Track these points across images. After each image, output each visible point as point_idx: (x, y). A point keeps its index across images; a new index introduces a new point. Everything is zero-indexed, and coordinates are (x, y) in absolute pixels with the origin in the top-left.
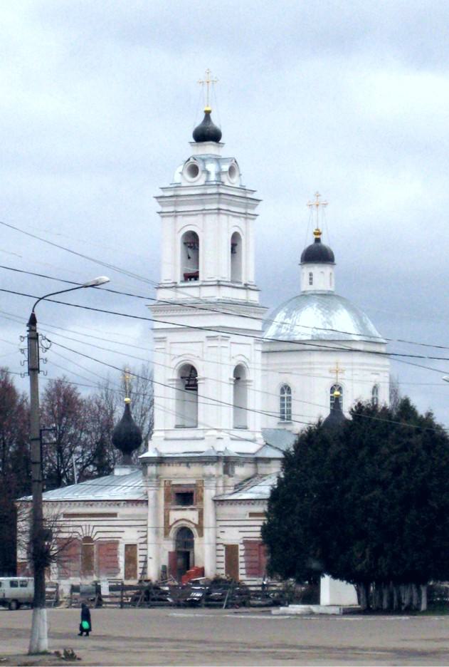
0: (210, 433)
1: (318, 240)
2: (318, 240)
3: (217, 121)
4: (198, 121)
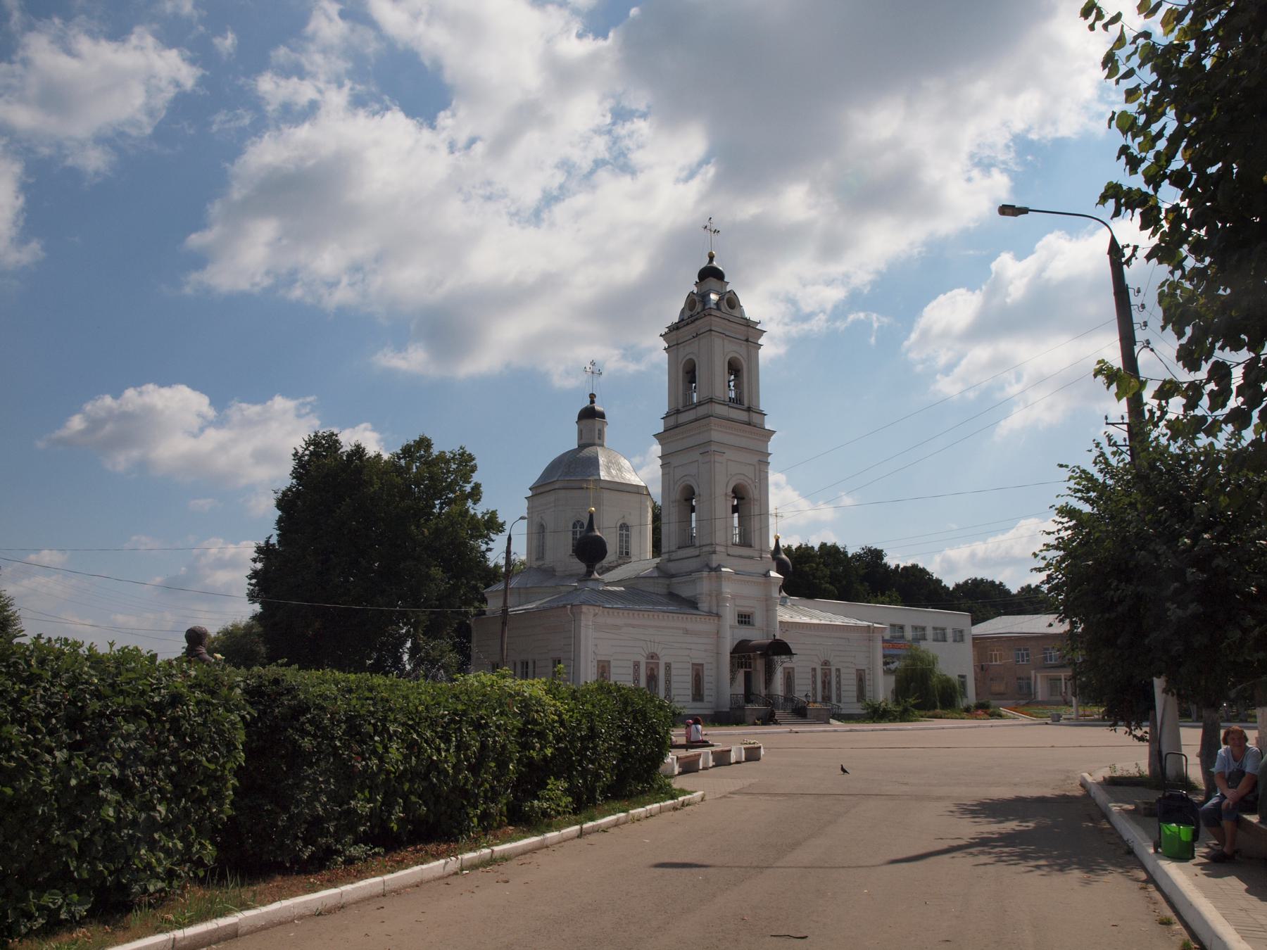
4: (704, 263)
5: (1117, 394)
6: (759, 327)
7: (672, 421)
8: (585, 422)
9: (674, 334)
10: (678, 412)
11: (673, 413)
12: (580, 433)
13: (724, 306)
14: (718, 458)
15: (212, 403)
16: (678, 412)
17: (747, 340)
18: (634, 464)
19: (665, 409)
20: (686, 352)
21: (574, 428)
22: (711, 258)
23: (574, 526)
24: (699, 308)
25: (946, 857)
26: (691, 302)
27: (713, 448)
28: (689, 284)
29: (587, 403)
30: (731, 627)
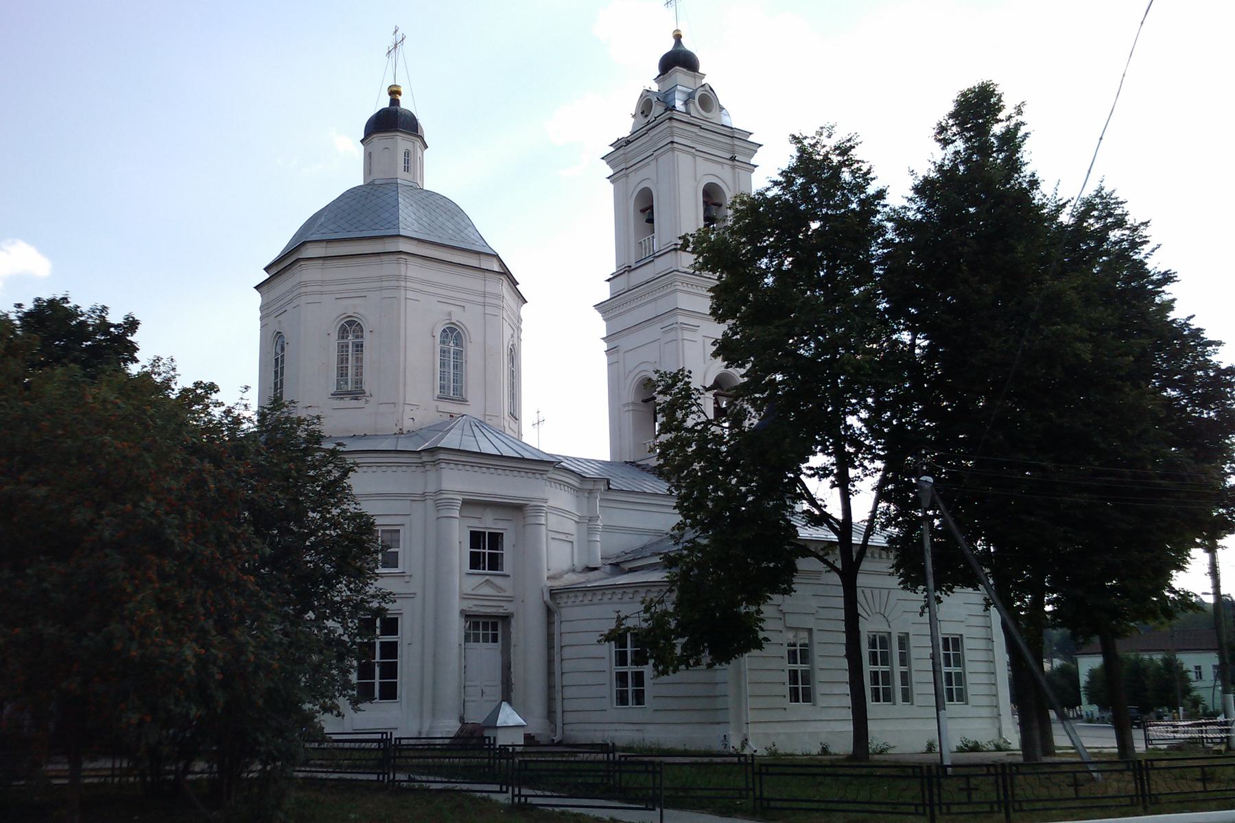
1: (395, 102)
2: (395, 102)
3: (688, 44)
4: (669, 46)
5: (1172, 308)
6: (751, 139)
7: (622, 282)
8: (379, 140)
9: (623, 156)
10: (629, 269)
11: (625, 270)
12: (369, 157)
13: (696, 109)
14: (687, 335)
15: (1088, 683)
16: (629, 269)
17: (733, 159)
18: (937, 812)
19: (610, 266)
20: (636, 181)
21: (358, 152)
22: (678, 37)
24: (657, 110)
25: (421, 261)
26: (646, 105)
27: (681, 319)
28: (647, 77)
29: (385, 103)
30: (450, 314)
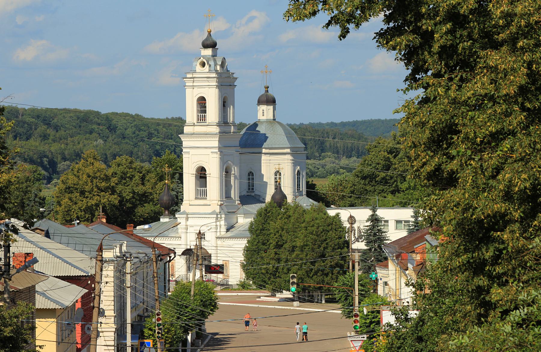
0: (214, 202)
10: (194, 125)
23: (249, 175)
